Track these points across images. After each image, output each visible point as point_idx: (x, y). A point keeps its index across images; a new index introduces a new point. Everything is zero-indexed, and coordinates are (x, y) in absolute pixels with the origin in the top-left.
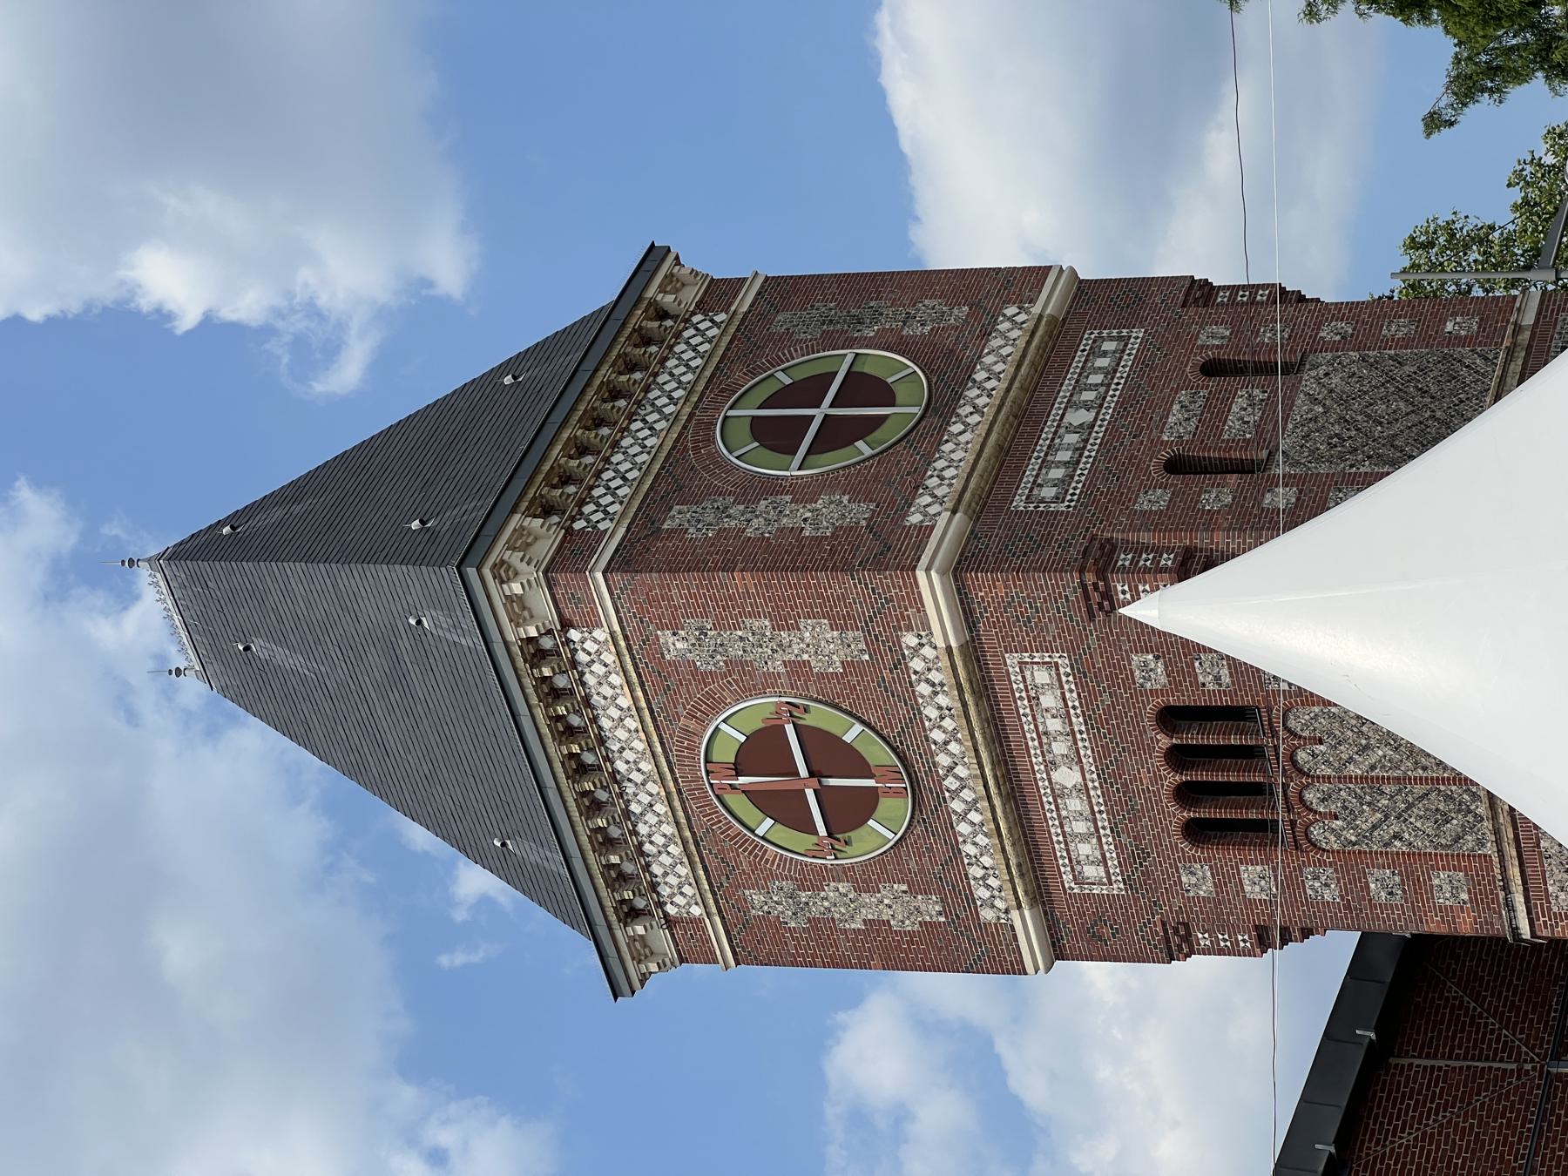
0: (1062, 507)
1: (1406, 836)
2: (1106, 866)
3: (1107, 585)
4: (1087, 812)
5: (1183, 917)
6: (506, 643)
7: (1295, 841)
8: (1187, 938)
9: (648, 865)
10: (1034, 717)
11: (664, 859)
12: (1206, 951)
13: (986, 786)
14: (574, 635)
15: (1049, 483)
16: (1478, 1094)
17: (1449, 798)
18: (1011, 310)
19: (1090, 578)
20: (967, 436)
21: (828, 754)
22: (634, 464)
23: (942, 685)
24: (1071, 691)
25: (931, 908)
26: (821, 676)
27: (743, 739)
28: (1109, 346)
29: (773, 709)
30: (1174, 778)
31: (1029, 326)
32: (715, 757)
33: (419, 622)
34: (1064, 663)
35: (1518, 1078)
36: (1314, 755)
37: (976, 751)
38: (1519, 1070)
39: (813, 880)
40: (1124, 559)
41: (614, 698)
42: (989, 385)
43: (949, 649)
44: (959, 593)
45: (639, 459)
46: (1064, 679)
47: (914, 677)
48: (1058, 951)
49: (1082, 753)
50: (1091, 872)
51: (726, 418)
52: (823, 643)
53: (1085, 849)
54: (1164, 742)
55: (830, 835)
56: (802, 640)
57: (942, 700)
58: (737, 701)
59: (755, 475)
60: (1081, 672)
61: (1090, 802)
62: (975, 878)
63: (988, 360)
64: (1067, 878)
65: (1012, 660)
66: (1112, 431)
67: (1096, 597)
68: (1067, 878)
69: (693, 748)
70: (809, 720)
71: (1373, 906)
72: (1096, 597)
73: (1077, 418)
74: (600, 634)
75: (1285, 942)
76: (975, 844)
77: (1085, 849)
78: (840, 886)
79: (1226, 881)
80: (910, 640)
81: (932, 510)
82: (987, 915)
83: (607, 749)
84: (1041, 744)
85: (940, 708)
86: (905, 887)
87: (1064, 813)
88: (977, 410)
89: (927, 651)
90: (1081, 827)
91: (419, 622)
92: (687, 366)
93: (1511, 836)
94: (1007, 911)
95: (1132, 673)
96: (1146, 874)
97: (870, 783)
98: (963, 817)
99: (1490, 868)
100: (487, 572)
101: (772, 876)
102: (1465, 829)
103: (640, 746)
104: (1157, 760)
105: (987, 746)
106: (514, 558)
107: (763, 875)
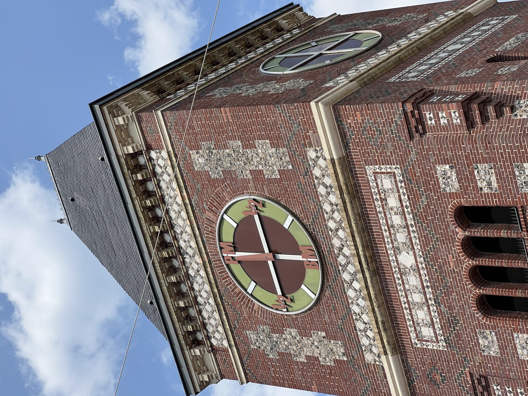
2: (434, 329)
3: (420, 114)
5: (482, 371)
14: (153, 154)
19: (409, 107)
24: (404, 194)
26: (270, 181)
30: (469, 263)
39: (278, 325)
43: (332, 160)
44: (337, 121)
46: (399, 185)
47: (316, 181)
49: (414, 241)
52: (268, 158)
54: (461, 234)
55: (283, 294)
56: (257, 154)
60: (409, 179)
61: (421, 279)
62: (360, 330)
65: (370, 170)
67: (413, 122)
68: (413, 335)
69: (213, 232)
70: (267, 212)
72: (413, 122)
76: (358, 305)
78: (292, 330)
80: (312, 154)
83: (175, 232)
84: (390, 233)
86: (324, 334)
87: (407, 287)
89: (321, 162)
95: (438, 180)
97: (299, 258)
101: (258, 322)
104: (457, 248)
105: (359, 233)
107: (253, 322)
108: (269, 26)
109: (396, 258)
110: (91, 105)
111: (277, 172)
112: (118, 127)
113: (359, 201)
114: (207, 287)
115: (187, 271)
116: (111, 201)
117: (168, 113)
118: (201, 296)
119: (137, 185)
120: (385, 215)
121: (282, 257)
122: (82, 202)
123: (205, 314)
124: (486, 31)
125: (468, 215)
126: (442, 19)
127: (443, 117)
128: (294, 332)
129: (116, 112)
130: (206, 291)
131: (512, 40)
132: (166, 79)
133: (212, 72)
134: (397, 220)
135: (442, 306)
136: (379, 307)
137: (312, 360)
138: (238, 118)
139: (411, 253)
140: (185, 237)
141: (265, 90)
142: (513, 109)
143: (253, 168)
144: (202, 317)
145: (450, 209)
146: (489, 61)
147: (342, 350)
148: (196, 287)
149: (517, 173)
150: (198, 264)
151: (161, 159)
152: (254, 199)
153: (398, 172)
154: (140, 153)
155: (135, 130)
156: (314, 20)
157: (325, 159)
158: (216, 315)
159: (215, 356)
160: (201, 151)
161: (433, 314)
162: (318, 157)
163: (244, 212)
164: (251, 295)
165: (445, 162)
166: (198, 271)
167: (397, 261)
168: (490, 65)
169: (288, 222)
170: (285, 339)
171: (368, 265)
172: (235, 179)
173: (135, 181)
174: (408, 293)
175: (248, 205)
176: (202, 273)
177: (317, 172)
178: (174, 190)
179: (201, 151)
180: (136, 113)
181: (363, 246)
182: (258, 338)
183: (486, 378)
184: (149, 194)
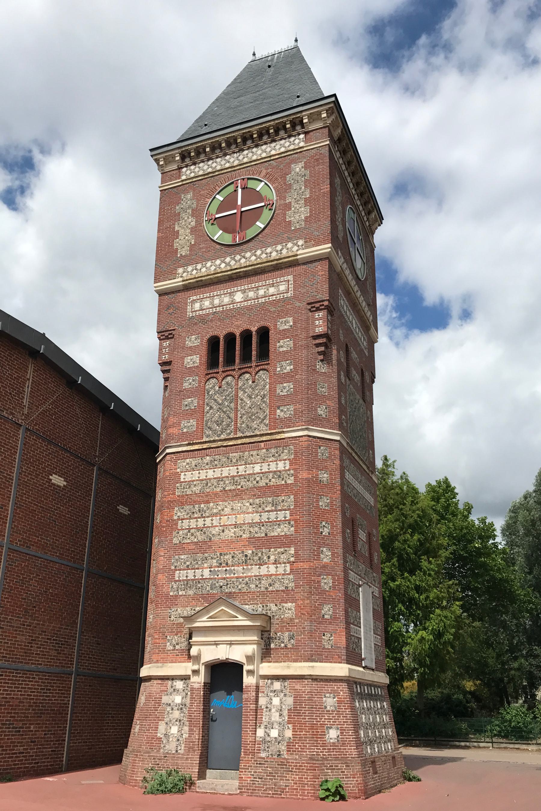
1: (211, 411)
2: (199, 310)
3: (322, 309)
4: (223, 304)
6: (301, 112)
7: (209, 374)
8: (167, 338)
10: (265, 285)
12: (161, 345)
13: (236, 269)
14: (302, 136)
16: (90, 440)
17: (228, 425)
19: (326, 303)
24: (276, 298)
26: (285, 214)
32: (249, 181)
35: (94, 455)
36: (247, 380)
37: (252, 265)
39: (196, 213)
43: (297, 255)
46: (282, 295)
47: (284, 244)
48: (162, 294)
52: (299, 214)
54: (254, 329)
55: (216, 219)
58: (274, 188)
60: (285, 301)
62: (196, 266)
64: (195, 298)
65: (290, 278)
67: (317, 305)
68: (195, 298)
69: (253, 174)
70: (266, 212)
71: (181, 399)
72: (317, 305)
75: (164, 372)
76: (211, 266)
78: (194, 222)
79: (192, 350)
80: (300, 242)
83: (253, 148)
84: (253, 288)
86: (193, 243)
87: (223, 296)
93: (212, 446)
98: (223, 262)
99: (197, 439)
101: (198, 200)
102: (215, 432)
104: (245, 327)
107: (198, 197)
108: (372, 207)
109: (239, 291)
110: (335, 95)
111: (290, 219)
112: (320, 113)
113: (272, 270)
114: (219, 168)
115: (229, 155)
116: (271, 100)
117: (327, 148)
118: (213, 163)
119: (283, 124)
120: (264, 286)
122: (268, 74)
123: (201, 165)
124: (361, 340)
125: (264, 334)
126: (369, 314)
127: (319, 322)
129: (330, 112)
130: (216, 167)
131: (356, 356)
132: (347, 144)
133: (348, 173)
134: (261, 292)
135: (212, 316)
136: (211, 279)
138: (324, 196)
139: (242, 300)
140: (250, 155)
141: (338, 212)
142: (322, 361)
143: (293, 204)
144: (200, 163)
146: (347, 345)
147: (183, 254)
148: (219, 160)
149: (287, 362)
150: (233, 162)
151: (298, 141)
152: (273, 203)
153: (289, 295)
154: (303, 127)
155: (319, 125)
156: (373, 233)
157: (297, 251)
158: (201, 173)
159: (176, 170)
160: (303, 169)
161: (208, 310)
162: (298, 246)
164: (215, 197)
165: (294, 323)
166: (229, 162)
167: (238, 291)
168: (345, 346)
169: (260, 225)
170: (188, 218)
171: (235, 273)
172: (286, 192)
173: (285, 123)
174: (219, 297)
175: (270, 199)
176: (228, 165)
177: (290, 245)
178: (279, 149)
179: (303, 169)
180: (327, 126)
181: (246, 271)
182: (188, 199)
183: (172, 338)
184: (277, 132)
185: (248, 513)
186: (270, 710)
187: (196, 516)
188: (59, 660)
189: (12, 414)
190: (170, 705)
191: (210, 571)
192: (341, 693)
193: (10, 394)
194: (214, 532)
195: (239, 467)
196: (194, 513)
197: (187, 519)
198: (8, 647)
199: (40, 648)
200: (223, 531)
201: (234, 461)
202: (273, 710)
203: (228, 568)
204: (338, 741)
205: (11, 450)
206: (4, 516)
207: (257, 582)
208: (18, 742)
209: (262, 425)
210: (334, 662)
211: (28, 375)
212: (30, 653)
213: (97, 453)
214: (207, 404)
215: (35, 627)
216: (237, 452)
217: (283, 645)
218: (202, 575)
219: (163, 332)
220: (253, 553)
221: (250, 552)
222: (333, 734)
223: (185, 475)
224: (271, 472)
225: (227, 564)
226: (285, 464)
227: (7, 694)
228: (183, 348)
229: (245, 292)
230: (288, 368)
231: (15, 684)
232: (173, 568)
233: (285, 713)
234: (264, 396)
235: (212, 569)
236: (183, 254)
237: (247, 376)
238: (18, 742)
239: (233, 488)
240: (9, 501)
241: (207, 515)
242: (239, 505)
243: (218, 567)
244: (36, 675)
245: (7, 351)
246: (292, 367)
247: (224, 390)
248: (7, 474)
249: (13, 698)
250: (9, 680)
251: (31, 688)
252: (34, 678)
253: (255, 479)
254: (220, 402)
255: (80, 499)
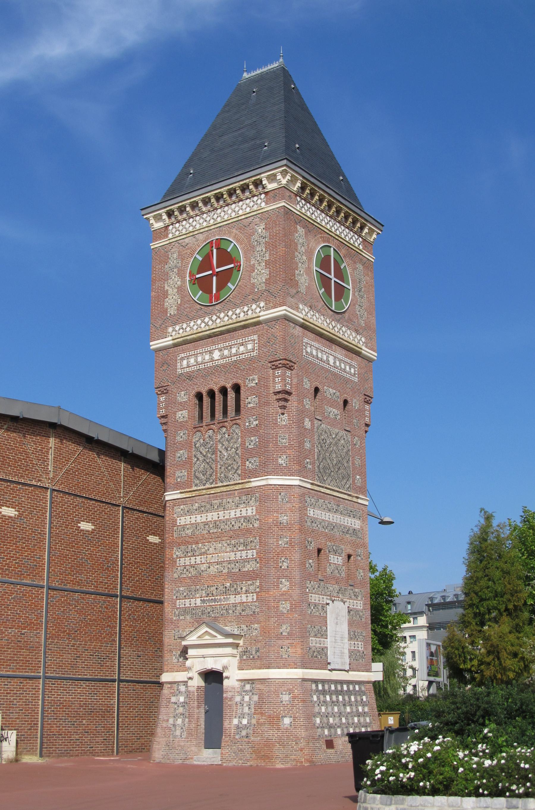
0: (304, 354)
1: (198, 462)
3: (280, 367)
4: (205, 361)
9: (185, 220)
11: (188, 225)
14: (263, 196)
15: (313, 349)
17: (211, 475)
18: (363, 339)
20: (326, 324)
21: (224, 278)
22: (317, 217)
23: (247, 314)
24: (245, 356)
25: (172, 311)
27: (229, 250)
28: (352, 371)
29: (239, 260)
31: (359, 345)
32: (222, 241)
33: (266, 146)
34: (255, 354)
35: (118, 497)
36: (224, 433)
37: (225, 326)
38: (121, 497)
40: (288, 373)
41: (242, 209)
42: (341, 331)
43: (259, 317)
45: (318, 219)
50: (185, 362)
51: (330, 247)
53: (192, 361)
57: (242, 314)
59: (314, 255)
60: (251, 360)
63: (348, 332)
64: (183, 355)
65: (255, 337)
66: (328, 371)
68: (183, 355)
70: (235, 271)
73: (332, 359)
74: (263, 204)
77: (192, 361)
79: (183, 406)
80: (262, 304)
81: (303, 312)
82: (170, 329)
85: (239, 314)
86: (179, 303)
87: (204, 354)
88: (334, 327)
90: (200, 359)
91: (266, 146)
92: (346, 235)
94: (171, 336)
96: (184, 381)
97: (214, 292)
98: (203, 321)
100: (285, 168)
101: (183, 260)
103: (226, 217)
104: (222, 383)
106: (288, 177)
121: (215, 278)
128: (179, 283)
137: (165, 294)
145: (240, 382)
163: (235, 258)
185: (227, 552)
186: (243, 705)
187: (189, 555)
188: (103, 671)
189: (39, 480)
190: (176, 703)
191: (201, 600)
192: (296, 691)
193: (37, 464)
194: (202, 569)
195: (219, 513)
196: (187, 552)
197: (183, 557)
198: (57, 663)
199: (84, 662)
200: (209, 568)
201: (216, 507)
202: (245, 705)
203: (213, 598)
204: (291, 726)
205: (42, 510)
206: (42, 564)
207: (234, 609)
208: (74, 732)
209: (236, 475)
210: (291, 668)
211: (51, 444)
212: (76, 667)
213: (122, 494)
214: (195, 456)
215: (78, 647)
216: (218, 500)
217: (251, 656)
218: (196, 604)
219: (160, 387)
220: (231, 584)
221: (229, 584)
222: (287, 721)
223: (180, 519)
224: (242, 517)
225: (212, 594)
226: (252, 509)
227: (60, 698)
228: (175, 403)
229: (221, 350)
230: (255, 423)
231: (66, 690)
232: (175, 597)
233: (252, 706)
234: (237, 449)
235: (202, 599)
236: (172, 313)
237: (224, 430)
238: (74, 732)
239: (215, 531)
240: (45, 551)
241: (197, 554)
242: (220, 545)
243: (207, 597)
244: (83, 683)
245: (30, 430)
246: (257, 422)
247: (207, 443)
248: (41, 531)
249: (66, 701)
250: (61, 687)
251: (80, 693)
252: (82, 686)
253: (231, 523)
254: (205, 454)
255: (109, 538)
